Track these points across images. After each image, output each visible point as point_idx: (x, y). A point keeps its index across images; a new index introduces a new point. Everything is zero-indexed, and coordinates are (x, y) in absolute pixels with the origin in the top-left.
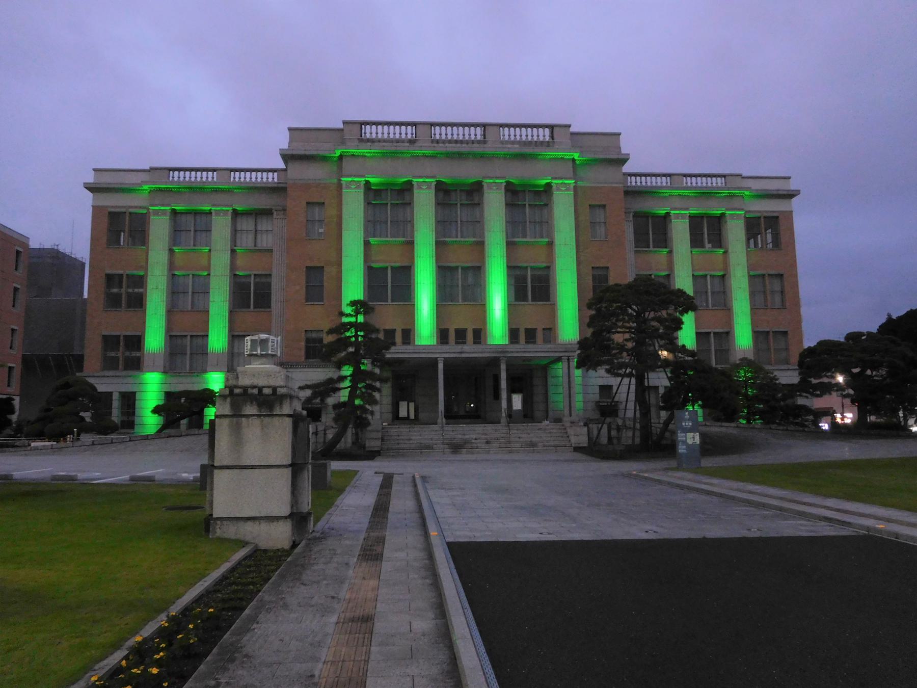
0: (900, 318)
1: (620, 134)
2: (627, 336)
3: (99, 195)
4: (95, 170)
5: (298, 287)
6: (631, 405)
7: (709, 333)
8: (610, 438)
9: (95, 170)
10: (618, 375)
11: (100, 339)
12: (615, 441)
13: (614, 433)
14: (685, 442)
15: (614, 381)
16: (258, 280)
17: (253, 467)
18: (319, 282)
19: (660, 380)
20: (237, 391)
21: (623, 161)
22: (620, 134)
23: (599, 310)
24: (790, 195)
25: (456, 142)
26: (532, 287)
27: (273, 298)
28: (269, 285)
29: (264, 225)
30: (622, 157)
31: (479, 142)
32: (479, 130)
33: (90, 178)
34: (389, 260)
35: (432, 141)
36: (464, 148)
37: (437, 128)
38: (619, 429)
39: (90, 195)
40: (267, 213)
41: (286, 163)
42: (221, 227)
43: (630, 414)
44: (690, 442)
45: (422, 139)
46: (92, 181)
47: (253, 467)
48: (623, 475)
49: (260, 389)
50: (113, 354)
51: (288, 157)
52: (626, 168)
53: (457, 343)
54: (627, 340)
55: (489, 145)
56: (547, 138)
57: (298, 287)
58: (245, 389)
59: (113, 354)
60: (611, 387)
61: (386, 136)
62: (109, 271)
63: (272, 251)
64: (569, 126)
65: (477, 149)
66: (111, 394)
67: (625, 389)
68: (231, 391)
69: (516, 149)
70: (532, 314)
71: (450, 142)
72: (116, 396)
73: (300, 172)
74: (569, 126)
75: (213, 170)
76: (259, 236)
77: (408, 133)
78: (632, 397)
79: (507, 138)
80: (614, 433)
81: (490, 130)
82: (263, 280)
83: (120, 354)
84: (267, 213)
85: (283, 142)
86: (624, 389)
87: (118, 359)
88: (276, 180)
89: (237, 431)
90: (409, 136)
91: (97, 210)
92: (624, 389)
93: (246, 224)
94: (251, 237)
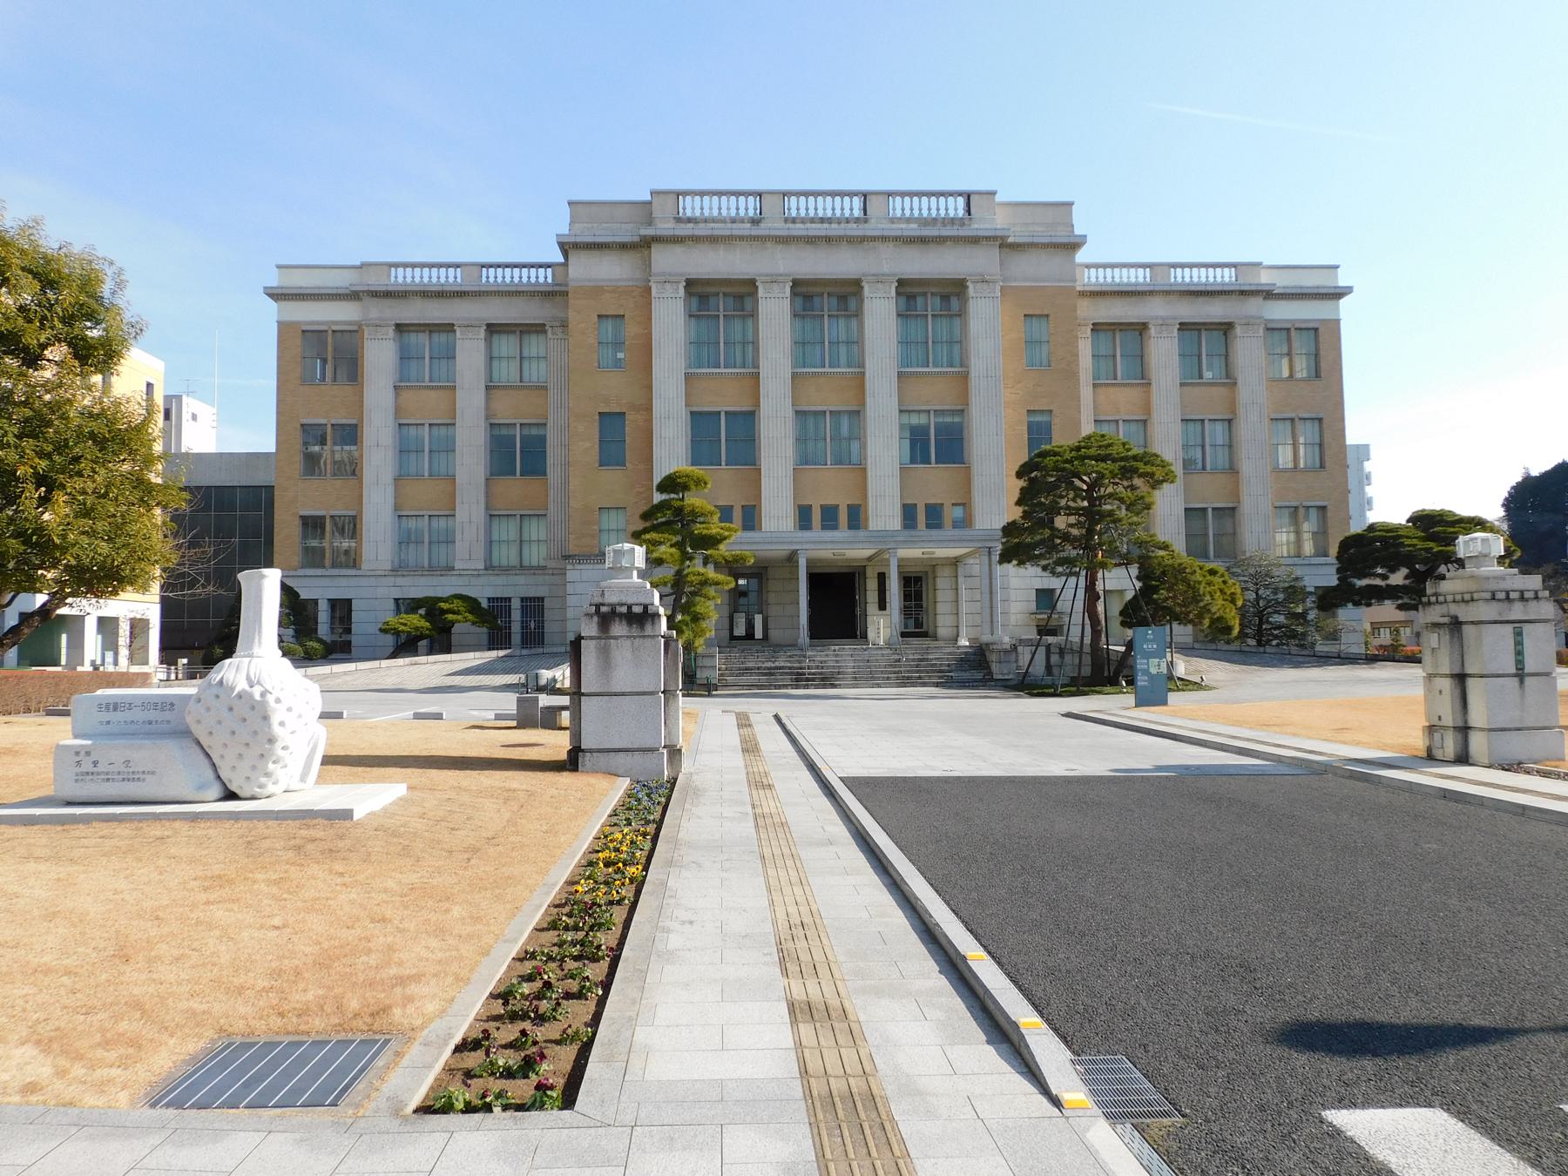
0: (1546, 476)
1: (1071, 204)
2: (1072, 519)
3: (284, 303)
4: (279, 267)
5: (587, 444)
6: (1077, 618)
7: (1204, 510)
8: (1049, 667)
9: (279, 267)
10: (1060, 575)
11: (298, 522)
12: (1055, 671)
13: (1055, 659)
14: (1146, 672)
15: (1055, 583)
16: (526, 432)
17: (623, 694)
18: (618, 435)
19: (1120, 581)
20: (604, 609)
21: (1074, 246)
22: (1071, 204)
23: (1031, 481)
24: (1337, 294)
25: (822, 220)
26: (937, 443)
27: (550, 461)
28: (542, 440)
29: (534, 345)
30: (1072, 240)
31: (857, 220)
32: (857, 202)
33: (274, 280)
34: (724, 400)
35: (786, 220)
36: (834, 230)
37: (793, 199)
38: (1062, 652)
39: (272, 305)
40: (539, 329)
41: (565, 254)
42: (470, 353)
43: (1075, 632)
44: (1153, 671)
45: (768, 223)
46: (275, 284)
47: (623, 694)
48: (1069, 715)
49: (630, 607)
50: (314, 543)
51: (565, 248)
52: (1081, 256)
53: (824, 527)
54: (1071, 526)
55: (872, 224)
56: (961, 212)
57: (587, 444)
58: (613, 606)
59: (314, 543)
60: (1053, 591)
61: (715, 213)
62: (305, 421)
63: (545, 388)
64: (993, 193)
65: (854, 230)
66: (316, 602)
67: (1070, 591)
68: (598, 612)
69: (913, 230)
70: (935, 482)
71: (812, 221)
72: (323, 607)
73: (584, 269)
74: (993, 193)
75: (457, 266)
76: (526, 364)
77: (749, 207)
78: (1079, 605)
79: (899, 213)
80: (1055, 659)
81: (872, 200)
82: (534, 431)
83: (326, 544)
84: (539, 329)
85: (561, 224)
86: (1068, 594)
87: (323, 550)
88: (550, 280)
89: (605, 653)
90: (751, 213)
91: (284, 328)
92: (1068, 594)
93: (506, 345)
94: (515, 365)
